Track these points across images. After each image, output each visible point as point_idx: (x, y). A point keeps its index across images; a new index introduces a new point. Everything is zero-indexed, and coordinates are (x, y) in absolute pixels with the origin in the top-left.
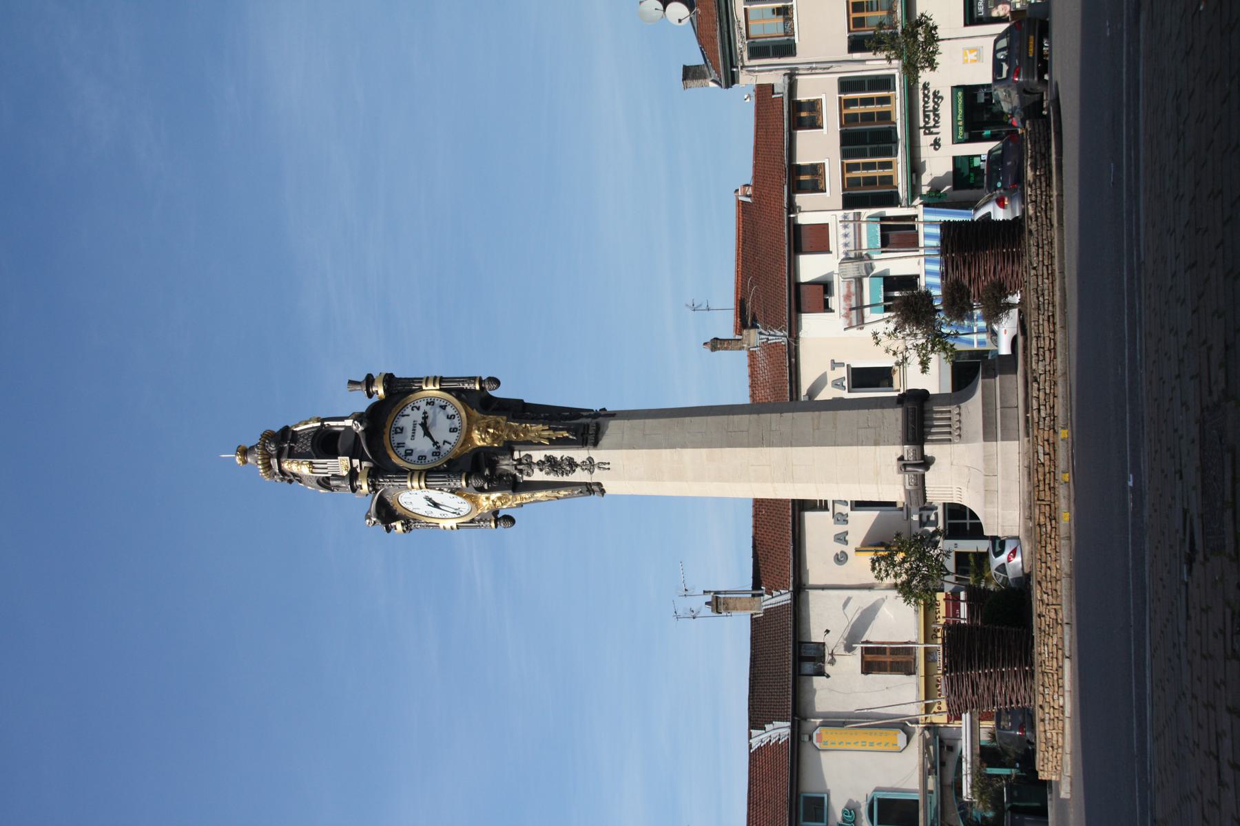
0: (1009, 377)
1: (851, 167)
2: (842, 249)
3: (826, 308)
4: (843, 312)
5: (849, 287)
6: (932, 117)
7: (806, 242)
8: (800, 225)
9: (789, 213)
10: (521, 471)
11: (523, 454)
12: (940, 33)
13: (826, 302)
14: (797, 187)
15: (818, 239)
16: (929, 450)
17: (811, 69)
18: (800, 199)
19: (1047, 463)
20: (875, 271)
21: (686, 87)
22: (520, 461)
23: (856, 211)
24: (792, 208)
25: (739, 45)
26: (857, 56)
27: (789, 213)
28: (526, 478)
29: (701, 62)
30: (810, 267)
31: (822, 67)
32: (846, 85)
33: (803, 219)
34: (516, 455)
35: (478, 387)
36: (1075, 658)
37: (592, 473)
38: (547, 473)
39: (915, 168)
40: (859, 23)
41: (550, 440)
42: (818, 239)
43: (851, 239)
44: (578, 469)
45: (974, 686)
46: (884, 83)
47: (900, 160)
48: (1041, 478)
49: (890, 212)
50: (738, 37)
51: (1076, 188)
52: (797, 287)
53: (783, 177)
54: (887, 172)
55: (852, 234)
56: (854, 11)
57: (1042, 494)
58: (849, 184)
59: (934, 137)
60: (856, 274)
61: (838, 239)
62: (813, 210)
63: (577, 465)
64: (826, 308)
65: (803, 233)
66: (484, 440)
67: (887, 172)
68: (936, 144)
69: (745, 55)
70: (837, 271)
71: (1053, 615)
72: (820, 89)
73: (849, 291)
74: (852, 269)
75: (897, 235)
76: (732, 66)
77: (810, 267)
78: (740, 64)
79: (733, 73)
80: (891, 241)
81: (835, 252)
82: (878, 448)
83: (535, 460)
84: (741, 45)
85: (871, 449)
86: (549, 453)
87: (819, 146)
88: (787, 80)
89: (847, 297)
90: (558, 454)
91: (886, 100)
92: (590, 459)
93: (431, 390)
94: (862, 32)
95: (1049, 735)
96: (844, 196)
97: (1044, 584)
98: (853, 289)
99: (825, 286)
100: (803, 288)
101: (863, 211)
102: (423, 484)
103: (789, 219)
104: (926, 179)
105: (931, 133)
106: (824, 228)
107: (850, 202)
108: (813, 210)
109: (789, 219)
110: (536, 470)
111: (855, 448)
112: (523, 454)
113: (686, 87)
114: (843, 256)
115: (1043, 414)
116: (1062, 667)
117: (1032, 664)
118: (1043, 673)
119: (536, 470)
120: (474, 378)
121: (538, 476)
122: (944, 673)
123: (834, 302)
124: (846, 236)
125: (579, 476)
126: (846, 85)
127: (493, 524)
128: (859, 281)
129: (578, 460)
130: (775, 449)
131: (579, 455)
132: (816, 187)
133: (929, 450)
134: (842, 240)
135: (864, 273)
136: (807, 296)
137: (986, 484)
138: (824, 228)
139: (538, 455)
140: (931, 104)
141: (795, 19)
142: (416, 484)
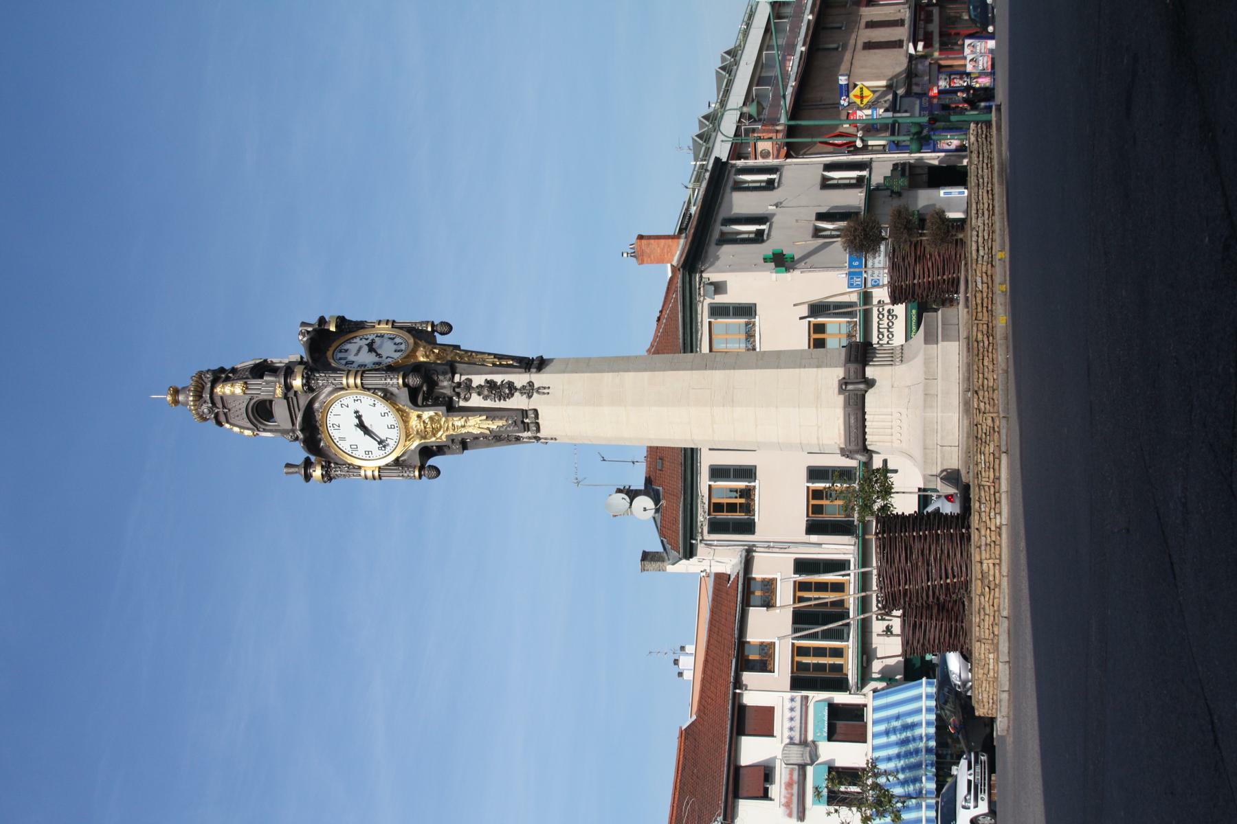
0: (950, 311)
1: (801, 599)
2: (787, 733)
3: (765, 796)
4: (783, 801)
5: (791, 774)
6: (886, 333)
7: (749, 723)
8: (745, 706)
9: (735, 688)
10: (458, 395)
11: (464, 378)
12: (896, 489)
13: (766, 790)
14: (745, 664)
15: (763, 722)
16: (870, 372)
17: (769, 547)
18: (747, 677)
19: (985, 289)
20: (820, 760)
21: (643, 570)
22: (459, 384)
23: (804, 693)
24: (738, 683)
25: (700, 518)
26: (814, 538)
27: (735, 688)
28: (462, 403)
29: (661, 550)
30: (752, 750)
31: (783, 546)
32: (802, 566)
33: (751, 699)
34: (457, 378)
35: (430, 329)
36: (1016, 451)
37: (530, 397)
38: (485, 398)
39: (866, 653)
40: (817, 509)
41: (494, 365)
42: (763, 722)
43: (797, 723)
44: (517, 394)
45: (908, 550)
46: (840, 566)
47: (851, 646)
48: (979, 301)
49: (840, 698)
50: (700, 511)
51: (1037, 748)
52: (736, 771)
53: (733, 656)
54: (838, 661)
55: (798, 718)
56: (813, 498)
57: (980, 315)
58: (798, 668)
59: (886, 623)
60: (800, 761)
61: (781, 724)
62: (761, 691)
63: (516, 389)
64: (765, 796)
65: (748, 715)
66: (427, 357)
67: (838, 661)
68: (888, 631)
69: (706, 529)
70: (780, 756)
71: (989, 422)
72: (775, 567)
73: (791, 778)
74: (796, 755)
75: (845, 723)
76: (692, 538)
77: (752, 750)
78: (699, 538)
79: (692, 544)
80: (838, 730)
81: (777, 800)
82: (820, 370)
83: (474, 385)
84: (702, 518)
85: (813, 371)
86: (489, 377)
87: (770, 626)
88: (744, 554)
89: (789, 785)
90: (498, 378)
91: (838, 653)
92: (531, 384)
93: (384, 329)
94: (819, 517)
95: (985, 566)
96: (792, 678)
97: (981, 393)
98: (795, 777)
99: (766, 773)
100: (742, 771)
101: (810, 694)
102: (358, 381)
103: (735, 694)
104: (877, 666)
105: (883, 619)
106: (770, 711)
107: (798, 683)
108: (761, 691)
109: (735, 694)
110: (474, 395)
111: (797, 370)
112: (464, 378)
113: (643, 570)
114: (787, 741)
115: (981, 253)
116: (999, 478)
117: (969, 527)
118: (979, 486)
119: (474, 395)
120: (427, 322)
121: (476, 401)
122: (877, 534)
123: (776, 790)
124: (792, 709)
125: (518, 402)
126: (802, 566)
127: (417, 473)
128: (802, 767)
129: (518, 385)
130: (718, 372)
131: (520, 379)
132: (764, 665)
133: (870, 372)
134: (787, 724)
135: (808, 761)
136: (746, 783)
137: (926, 387)
138: (770, 711)
139: (478, 380)
140: (886, 321)
141: (757, 499)
142: (351, 381)
